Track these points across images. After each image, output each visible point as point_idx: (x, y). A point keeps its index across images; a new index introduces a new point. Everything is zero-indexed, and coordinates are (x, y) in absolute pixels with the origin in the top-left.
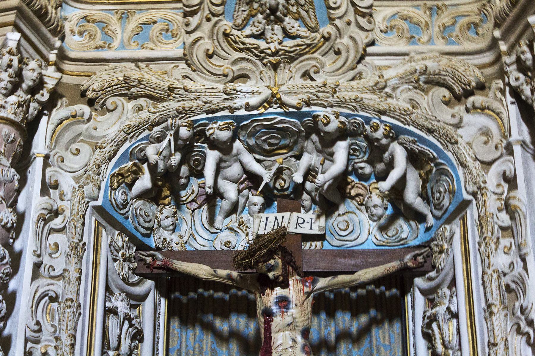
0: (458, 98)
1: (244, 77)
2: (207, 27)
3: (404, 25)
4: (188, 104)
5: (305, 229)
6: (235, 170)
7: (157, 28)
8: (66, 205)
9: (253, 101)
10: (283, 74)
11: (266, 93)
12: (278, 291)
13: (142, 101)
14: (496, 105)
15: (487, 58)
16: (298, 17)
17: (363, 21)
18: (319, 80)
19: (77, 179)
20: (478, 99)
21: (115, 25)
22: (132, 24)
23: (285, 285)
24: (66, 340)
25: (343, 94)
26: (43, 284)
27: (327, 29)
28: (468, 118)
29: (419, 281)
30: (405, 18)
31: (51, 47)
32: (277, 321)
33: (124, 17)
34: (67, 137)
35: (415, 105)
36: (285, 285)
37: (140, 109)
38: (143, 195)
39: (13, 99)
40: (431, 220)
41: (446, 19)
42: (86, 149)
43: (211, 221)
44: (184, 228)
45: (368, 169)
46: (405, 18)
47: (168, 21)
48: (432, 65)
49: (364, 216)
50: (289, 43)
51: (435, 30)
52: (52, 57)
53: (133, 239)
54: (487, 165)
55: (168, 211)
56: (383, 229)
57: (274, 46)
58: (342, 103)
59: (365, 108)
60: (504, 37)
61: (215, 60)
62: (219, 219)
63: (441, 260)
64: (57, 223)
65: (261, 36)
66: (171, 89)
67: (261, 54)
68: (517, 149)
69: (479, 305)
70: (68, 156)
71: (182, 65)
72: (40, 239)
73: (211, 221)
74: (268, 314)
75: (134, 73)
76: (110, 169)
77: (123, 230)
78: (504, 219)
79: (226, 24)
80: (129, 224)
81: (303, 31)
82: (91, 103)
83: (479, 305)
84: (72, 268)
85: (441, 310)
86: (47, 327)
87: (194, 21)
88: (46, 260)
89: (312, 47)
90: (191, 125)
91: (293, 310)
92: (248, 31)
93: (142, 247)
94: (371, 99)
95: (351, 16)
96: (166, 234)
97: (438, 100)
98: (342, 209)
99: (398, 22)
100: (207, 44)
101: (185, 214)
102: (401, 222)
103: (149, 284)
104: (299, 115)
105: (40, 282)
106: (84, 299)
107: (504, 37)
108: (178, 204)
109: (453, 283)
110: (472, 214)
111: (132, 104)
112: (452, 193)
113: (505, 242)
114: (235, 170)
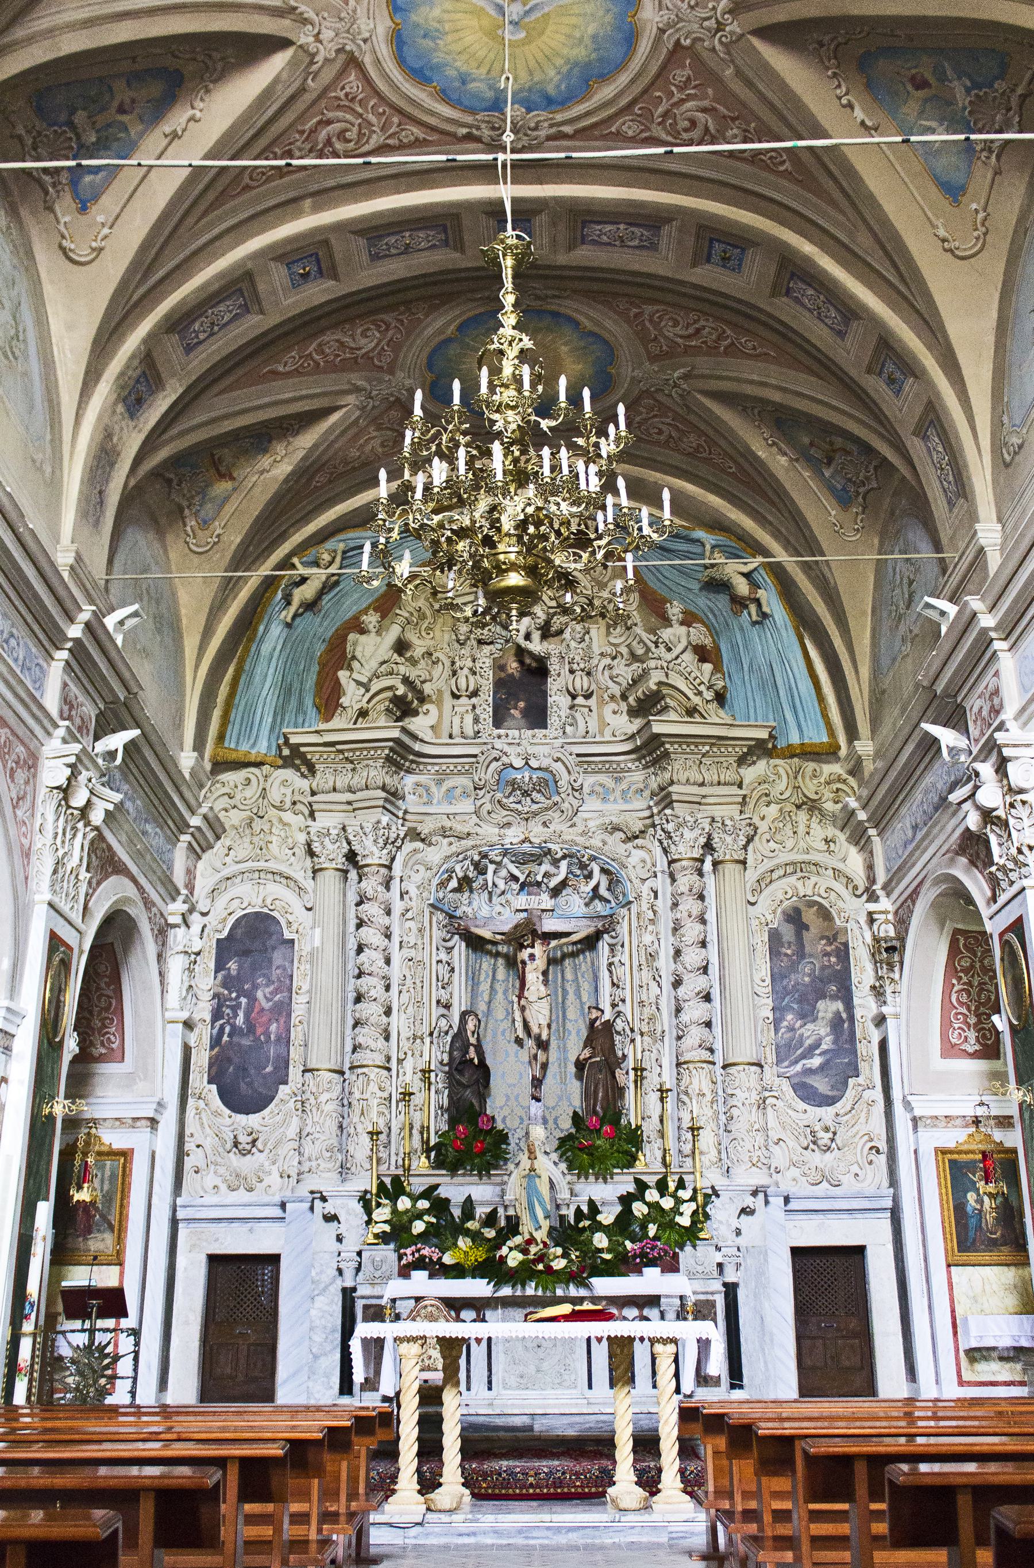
0: (629, 839)
1: (509, 825)
2: (488, 796)
3: (601, 790)
4: (478, 843)
5: (543, 907)
6: (503, 873)
7: (459, 791)
8: (413, 904)
9: (515, 841)
10: (531, 823)
11: (522, 837)
12: (529, 950)
13: (452, 839)
14: (649, 846)
15: (647, 813)
16: (539, 791)
17: (576, 794)
18: (552, 827)
19: (418, 887)
20: (639, 842)
21: (434, 789)
22: (444, 789)
23: (533, 947)
24: (420, 985)
25: (565, 837)
26: (407, 953)
27: (556, 798)
28: (634, 852)
29: (605, 936)
30: (601, 785)
31: (399, 809)
32: (529, 967)
33: (439, 783)
34: (410, 864)
35: (605, 843)
36: (533, 947)
37: (451, 844)
38: (454, 890)
39: (385, 851)
40: (613, 904)
41: (624, 786)
42: (422, 869)
43: (490, 900)
44: (475, 904)
45: (578, 872)
46: (601, 785)
47: (464, 787)
48: (615, 820)
49: (576, 897)
50: (535, 807)
51: (618, 793)
52: (400, 814)
53: (447, 913)
54: (644, 880)
55: (467, 894)
56: (587, 905)
57: (526, 809)
58: (564, 842)
59: (576, 844)
60: (657, 804)
61: (493, 815)
62: (494, 898)
63: (618, 928)
64: (409, 915)
65: (519, 802)
66: (469, 834)
67: (519, 813)
68: (659, 875)
69: (635, 964)
70: (412, 873)
71: (474, 816)
72: (401, 926)
73: (490, 900)
74: (524, 963)
75: (448, 824)
76: (436, 881)
77: (442, 911)
78: (650, 913)
79: (499, 795)
80: (446, 908)
81: (542, 799)
82: (423, 840)
83: (635, 964)
84: (419, 942)
85: (616, 960)
86: (408, 977)
87: (481, 793)
88: (405, 939)
89: (547, 809)
90: (480, 853)
91: (538, 962)
92: (512, 799)
93: (451, 917)
94: (580, 840)
95: (570, 791)
96: (465, 908)
97: (618, 840)
98: (564, 893)
99: (598, 789)
100: (488, 807)
101: (475, 895)
102: (597, 901)
103: (457, 937)
104: (541, 848)
105: (404, 950)
106: (427, 960)
107: (657, 804)
108: (471, 891)
109: (622, 946)
110: (634, 908)
111: (447, 840)
112: (624, 895)
113: (650, 928)
114: (503, 873)
